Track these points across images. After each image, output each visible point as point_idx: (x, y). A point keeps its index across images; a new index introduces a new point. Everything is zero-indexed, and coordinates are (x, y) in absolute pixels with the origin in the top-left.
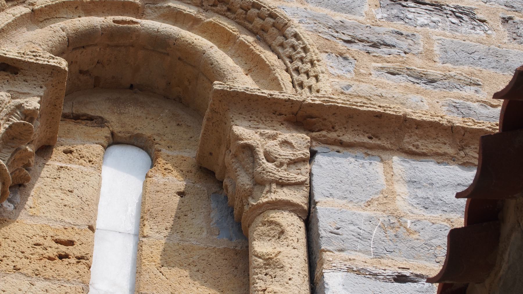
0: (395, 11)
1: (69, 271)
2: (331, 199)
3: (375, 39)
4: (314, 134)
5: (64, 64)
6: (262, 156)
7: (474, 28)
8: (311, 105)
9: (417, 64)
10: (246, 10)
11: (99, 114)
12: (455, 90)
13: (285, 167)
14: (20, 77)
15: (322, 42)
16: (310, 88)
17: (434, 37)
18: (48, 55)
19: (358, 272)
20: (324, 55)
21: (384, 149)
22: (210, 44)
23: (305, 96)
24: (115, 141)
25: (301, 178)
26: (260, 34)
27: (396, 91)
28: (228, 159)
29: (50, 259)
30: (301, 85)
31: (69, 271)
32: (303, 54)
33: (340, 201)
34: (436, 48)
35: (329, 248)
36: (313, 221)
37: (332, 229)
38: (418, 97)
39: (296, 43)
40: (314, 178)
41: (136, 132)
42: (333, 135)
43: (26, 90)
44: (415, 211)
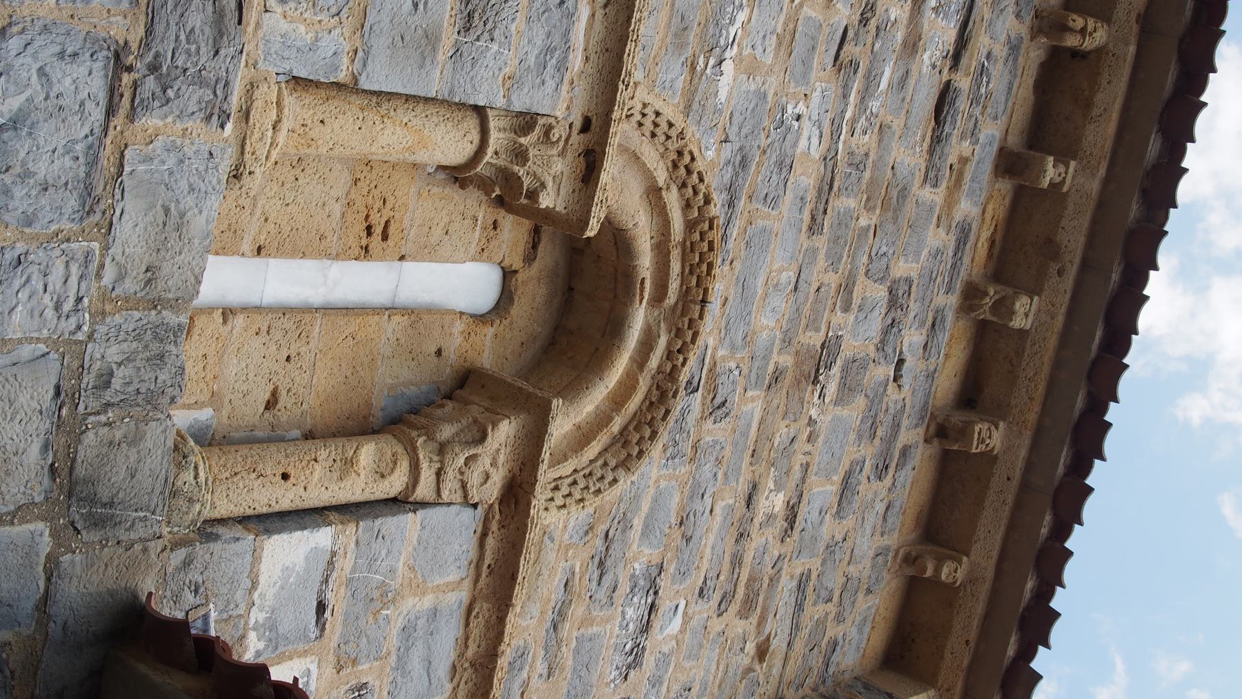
0: (642, 582)
1: (352, 238)
2: (419, 527)
3: (608, 563)
4: (497, 506)
5: (591, 232)
6: (472, 452)
7: (617, 668)
8: (529, 504)
9: (577, 611)
10: (650, 424)
11: (539, 256)
12: (543, 653)
13: (459, 477)
14: (579, 185)
15: (608, 507)
16: (552, 499)
17: (608, 627)
18: (603, 216)
19: (331, 563)
20: (591, 510)
21: (476, 581)
22: (611, 386)
23: (541, 495)
24: (508, 275)
25: (445, 496)
26: (622, 439)
27: (545, 590)
28: (475, 410)
29: (367, 216)
30: (556, 488)
31: (352, 238)
32: (592, 490)
33: (416, 537)
34: (595, 629)
35: (360, 530)
36: (395, 508)
37: (383, 532)
38: (536, 613)
39: (606, 481)
40: (445, 508)
41: (516, 298)
42: (494, 526)
43: (563, 192)
44: (400, 619)
